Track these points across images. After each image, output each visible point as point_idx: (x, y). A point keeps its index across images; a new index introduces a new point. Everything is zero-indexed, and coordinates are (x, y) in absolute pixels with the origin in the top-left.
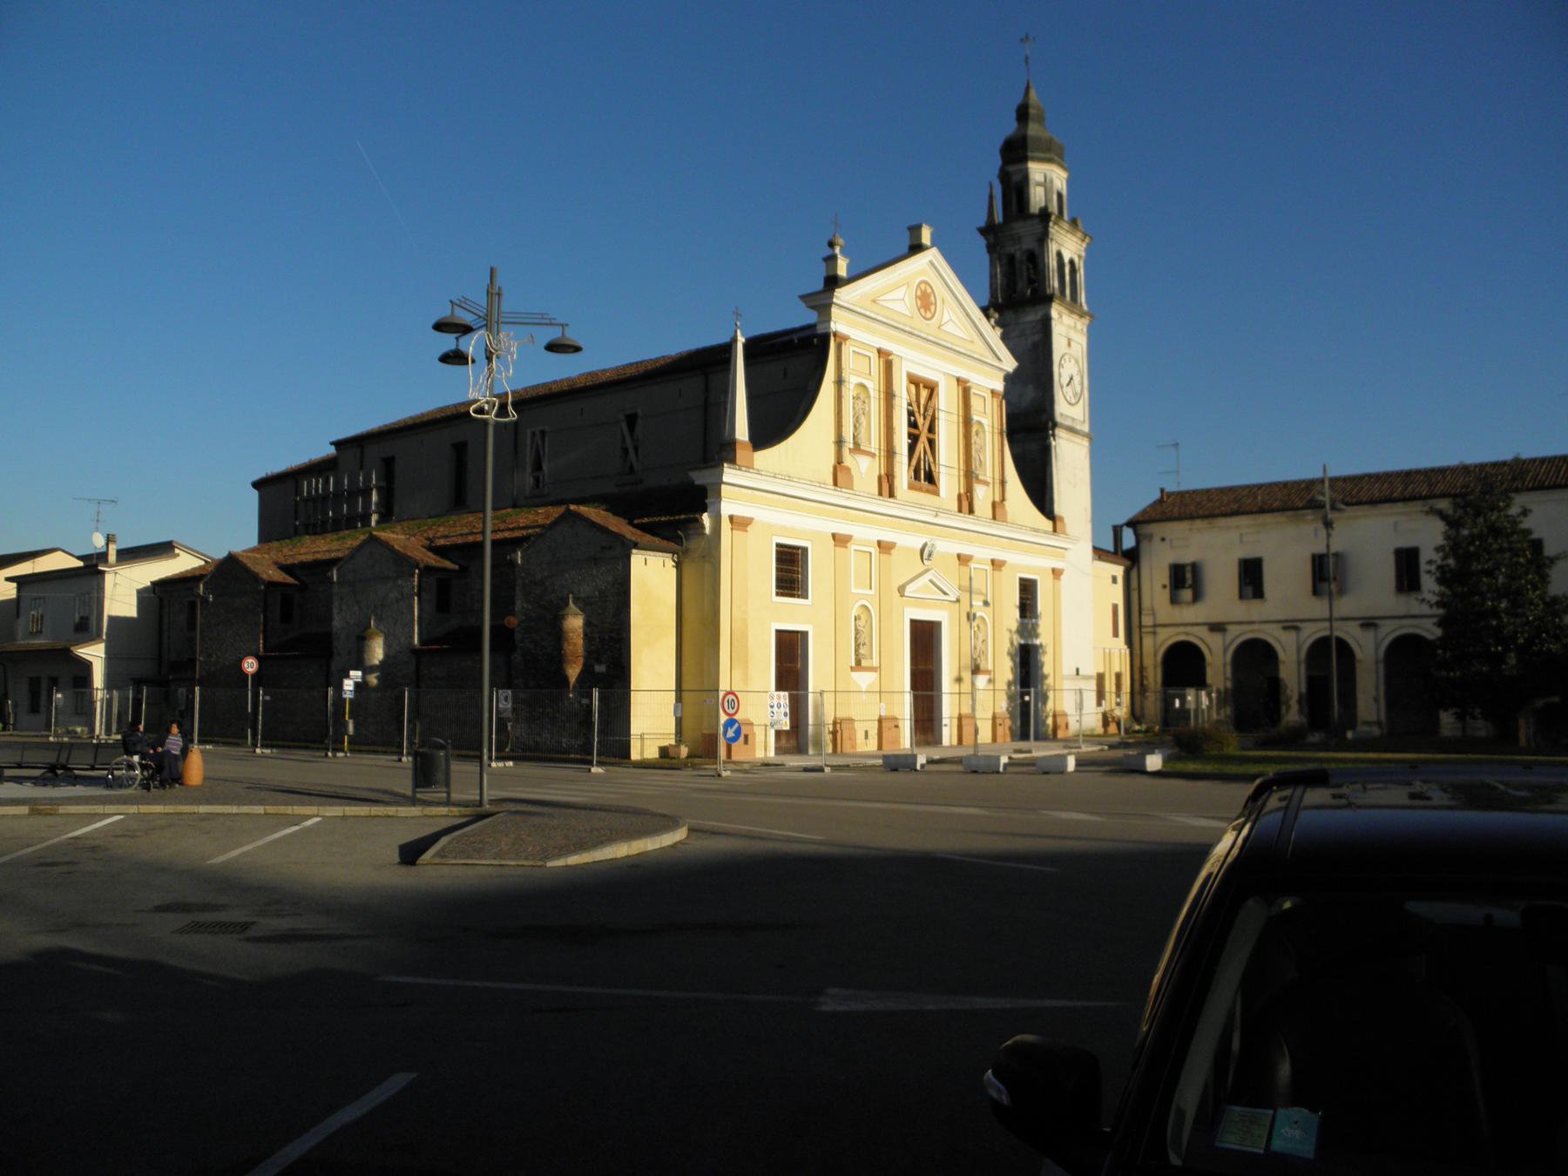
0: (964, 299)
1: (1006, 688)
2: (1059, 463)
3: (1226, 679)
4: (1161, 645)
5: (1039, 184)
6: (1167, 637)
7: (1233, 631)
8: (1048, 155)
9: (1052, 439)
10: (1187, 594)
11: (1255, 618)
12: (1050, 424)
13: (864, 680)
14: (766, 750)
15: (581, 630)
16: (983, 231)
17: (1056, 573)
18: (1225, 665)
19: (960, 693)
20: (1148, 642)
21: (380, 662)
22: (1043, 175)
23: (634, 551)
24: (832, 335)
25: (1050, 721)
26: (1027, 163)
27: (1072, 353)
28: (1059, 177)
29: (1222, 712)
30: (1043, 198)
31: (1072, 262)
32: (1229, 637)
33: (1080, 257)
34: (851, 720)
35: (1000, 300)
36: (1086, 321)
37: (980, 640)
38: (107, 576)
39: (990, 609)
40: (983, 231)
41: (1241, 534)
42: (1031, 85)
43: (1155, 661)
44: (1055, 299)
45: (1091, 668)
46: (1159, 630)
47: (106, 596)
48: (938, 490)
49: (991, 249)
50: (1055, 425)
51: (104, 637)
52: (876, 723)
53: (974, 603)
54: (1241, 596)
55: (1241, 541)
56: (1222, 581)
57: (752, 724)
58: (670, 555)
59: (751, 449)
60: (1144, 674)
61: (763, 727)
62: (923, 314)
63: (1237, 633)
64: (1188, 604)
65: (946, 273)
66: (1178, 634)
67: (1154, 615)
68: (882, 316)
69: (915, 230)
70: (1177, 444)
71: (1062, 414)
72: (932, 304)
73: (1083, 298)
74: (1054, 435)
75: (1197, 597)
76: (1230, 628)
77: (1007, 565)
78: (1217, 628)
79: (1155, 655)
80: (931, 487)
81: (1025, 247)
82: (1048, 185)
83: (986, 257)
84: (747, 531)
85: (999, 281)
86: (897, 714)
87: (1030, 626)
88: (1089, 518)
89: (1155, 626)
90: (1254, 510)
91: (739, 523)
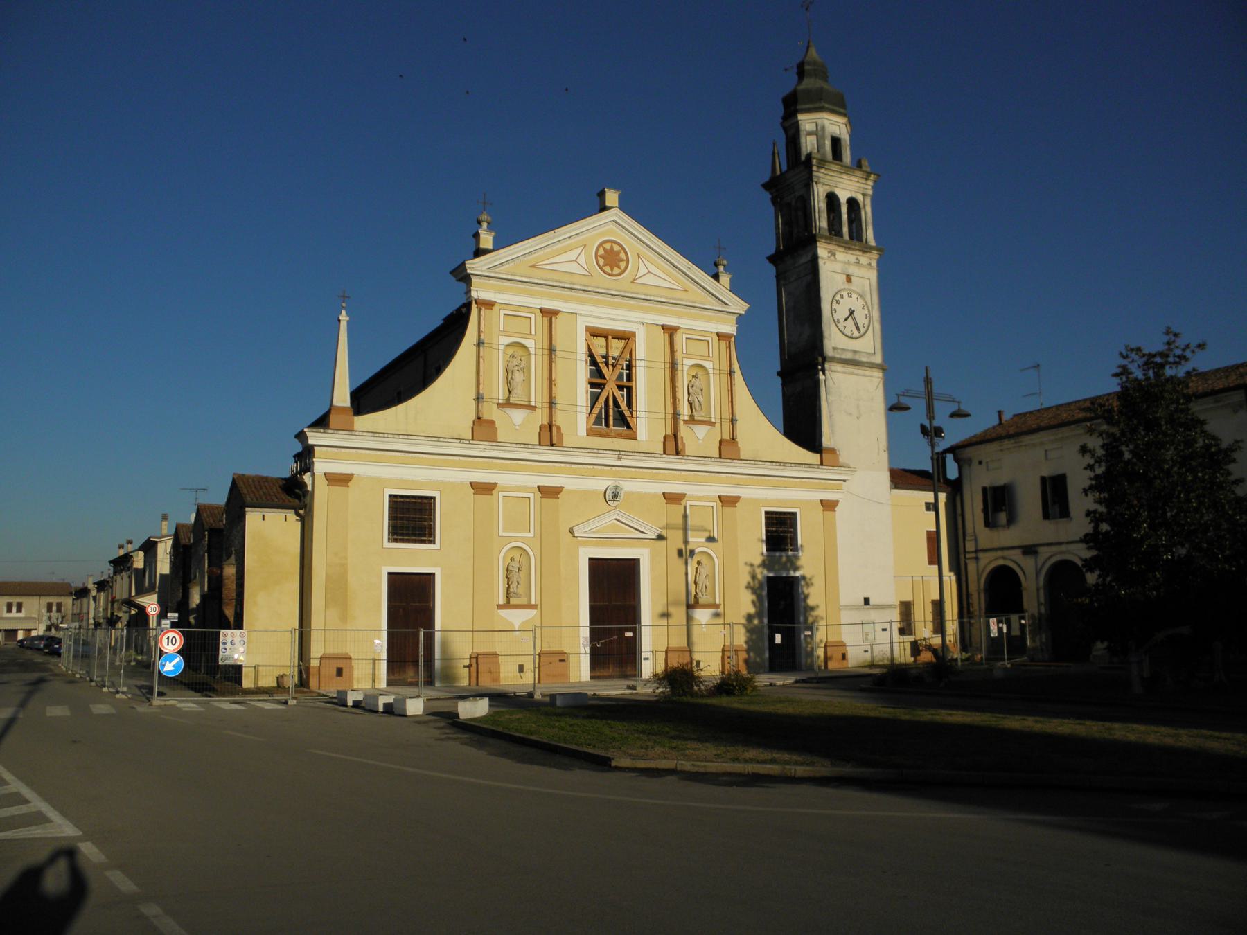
0: (667, 253)
1: (743, 621)
2: (831, 398)
3: (1040, 604)
4: (983, 571)
5: (810, 133)
6: (988, 562)
7: (1044, 552)
8: (817, 105)
9: (821, 373)
10: (1002, 517)
11: (1063, 539)
12: (820, 359)
13: (516, 618)
14: (374, 681)
15: (234, 578)
16: (766, 186)
18: (1038, 590)
19: (724, 624)
20: (972, 567)
21: (197, 605)
22: (815, 124)
23: (247, 509)
24: (474, 302)
25: (820, 652)
26: (797, 117)
27: (854, 288)
28: (835, 125)
29: (1037, 639)
30: (816, 146)
31: (852, 202)
32: (1041, 559)
33: (864, 195)
34: (495, 655)
35: (781, 248)
36: (874, 255)
37: (703, 575)
38: (159, 545)
39: (718, 546)
40: (766, 186)
41: (1046, 451)
42: (811, 44)
43: (979, 586)
44: (818, 239)
45: (889, 594)
46: (981, 555)
47: (158, 559)
48: (635, 433)
49: (774, 201)
50: (824, 359)
51: (157, 590)
52: (664, 653)
53: (690, 539)
54: (1046, 516)
55: (1046, 458)
56: (1029, 500)
57: (350, 658)
58: (293, 511)
59: (352, 413)
60: (970, 601)
63: (1049, 554)
64: (1004, 527)
65: (636, 230)
66: (996, 559)
67: (976, 540)
69: (602, 194)
70: (1038, 365)
71: (834, 349)
72: (605, 265)
73: (869, 234)
74: (823, 371)
75: (1011, 520)
76: (1041, 549)
78: (1029, 550)
79: (979, 580)
80: (629, 432)
81: (797, 194)
82: (820, 133)
83: (771, 209)
84: (348, 486)
85: (781, 231)
87: (784, 559)
88: (884, 443)
89: (977, 551)
91: (338, 480)
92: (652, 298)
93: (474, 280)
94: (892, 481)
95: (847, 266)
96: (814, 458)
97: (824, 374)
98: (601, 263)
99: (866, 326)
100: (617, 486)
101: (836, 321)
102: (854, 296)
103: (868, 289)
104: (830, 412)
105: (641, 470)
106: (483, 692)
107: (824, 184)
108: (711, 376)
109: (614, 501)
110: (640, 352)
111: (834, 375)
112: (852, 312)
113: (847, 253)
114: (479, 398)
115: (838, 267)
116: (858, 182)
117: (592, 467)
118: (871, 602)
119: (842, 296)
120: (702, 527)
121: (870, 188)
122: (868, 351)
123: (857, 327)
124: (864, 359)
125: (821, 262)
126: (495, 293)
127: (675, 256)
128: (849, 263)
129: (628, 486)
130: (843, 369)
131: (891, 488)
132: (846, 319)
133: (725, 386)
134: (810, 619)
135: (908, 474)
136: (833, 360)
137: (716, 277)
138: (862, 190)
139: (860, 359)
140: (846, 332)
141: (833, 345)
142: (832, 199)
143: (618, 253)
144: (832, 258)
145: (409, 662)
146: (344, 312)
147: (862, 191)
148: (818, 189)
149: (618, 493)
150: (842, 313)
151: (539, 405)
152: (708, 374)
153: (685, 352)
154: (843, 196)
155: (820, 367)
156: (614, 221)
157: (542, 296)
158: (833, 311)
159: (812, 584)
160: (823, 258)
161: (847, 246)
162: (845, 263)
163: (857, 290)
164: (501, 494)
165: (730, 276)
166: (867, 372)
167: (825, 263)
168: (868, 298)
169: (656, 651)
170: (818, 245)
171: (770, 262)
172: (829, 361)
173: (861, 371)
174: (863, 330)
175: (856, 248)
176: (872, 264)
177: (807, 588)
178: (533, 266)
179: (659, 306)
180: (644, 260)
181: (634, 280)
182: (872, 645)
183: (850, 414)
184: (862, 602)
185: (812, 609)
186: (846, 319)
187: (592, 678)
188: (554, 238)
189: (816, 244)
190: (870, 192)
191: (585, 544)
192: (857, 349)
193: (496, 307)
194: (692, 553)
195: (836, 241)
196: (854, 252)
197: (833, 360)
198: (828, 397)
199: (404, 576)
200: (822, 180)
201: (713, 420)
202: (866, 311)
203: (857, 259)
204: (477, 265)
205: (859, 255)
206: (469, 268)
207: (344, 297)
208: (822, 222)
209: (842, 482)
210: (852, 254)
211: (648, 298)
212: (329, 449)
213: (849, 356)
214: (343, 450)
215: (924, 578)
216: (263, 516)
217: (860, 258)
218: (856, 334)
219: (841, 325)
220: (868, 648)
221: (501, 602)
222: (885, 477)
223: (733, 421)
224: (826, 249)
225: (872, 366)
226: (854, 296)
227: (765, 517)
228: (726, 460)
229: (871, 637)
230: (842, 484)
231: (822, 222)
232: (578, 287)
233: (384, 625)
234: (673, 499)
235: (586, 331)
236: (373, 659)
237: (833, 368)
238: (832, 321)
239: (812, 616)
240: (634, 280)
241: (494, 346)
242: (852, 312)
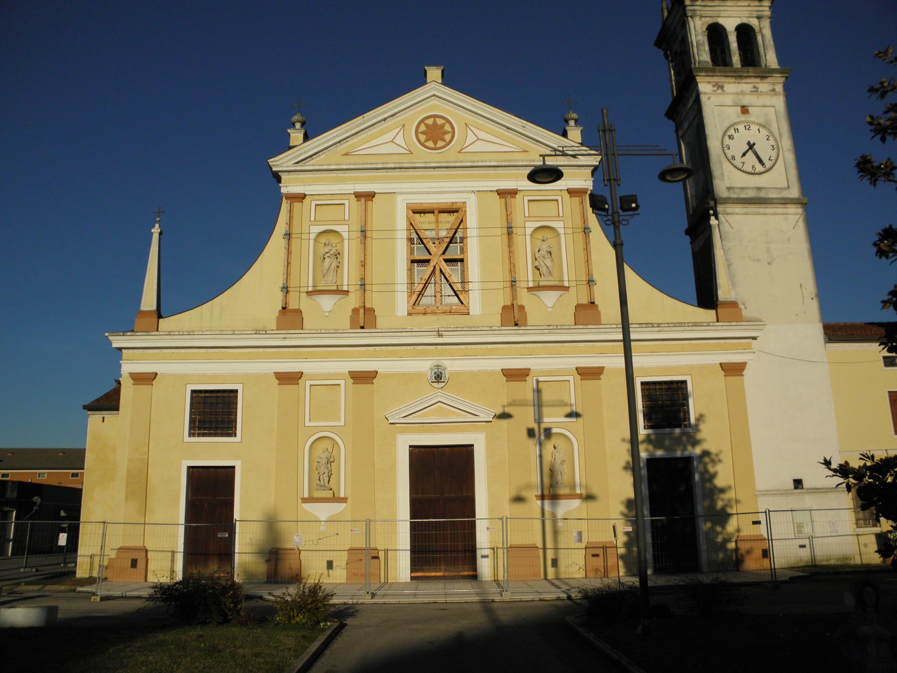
9: (713, 218)
12: (712, 203)
13: (323, 511)
17: (734, 370)
21: (852, 467)
33: (759, 18)
61: (170, 554)
62: (444, 143)
68: (436, 162)
71: (729, 189)
72: (435, 143)
73: (770, 58)
74: (716, 216)
77: (605, 371)
86: (379, 543)
90: (363, 270)
91: (145, 379)
92: (480, 164)
93: (284, 177)
94: (826, 334)
95: (740, 97)
96: (708, 315)
97: (717, 218)
98: (444, 143)
99: (773, 158)
100: (438, 366)
101: (730, 158)
102: (754, 128)
103: (772, 116)
104: (727, 260)
105: (473, 346)
106: (25, 601)
107: (701, 17)
108: (562, 237)
109: (438, 382)
110: (472, 220)
111: (731, 218)
112: (751, 146)
113: (738, 83)
114: (286, 289)
115: (728, 100)
116: (749, 6)
117: (412, 347)
118: (806, 484)
119: (736, 130)
120: (562, 401)
121: (768, 8)
122: (779, 186)
123: (760, 161)
124: (773, 195)
125: (703, 98)
126: (305, 185)
127: (505, 117)
128: (743, 93)
129: (451, 365)
130: (745, 210)
131: (826, 342)
132: (744, 154)
133: (581, 245)
134: (720, 504)
135: (871, 327)
136: (727, 201)
137: (564, 134)
138: (755, 13)
139: (766, 196)
140: (744, 168)
141: (728, 185)
142: (716, 33)
143: (435, 123)
144: (720, 91)
145: (213, 554)
146: (157, 226)
147: (755, 14)
148: (694, 23)
149: (441, 373)
150: (738, 146)
151: (351, 289)
152: (559, 235)
153: (527, 215)
154: (730, 24)
155: (711, 212)
156: (434, 95)
157: (355, 180)
158: (724, 148)
159: (720, 461)
160: (705, 93)
161: (737, 74)
162: (737, 94)
163: (758, 121)
164: (308, 383)
165: (581, 128)
166: (780, 210)
167: (709, 98)
168: (775, 128)
169: (388, 550)
170: (698, 81)
171: (669, 118)
172: (721, 203)
173: (769, 210)
174: (768, 164)
175: (751, 74)
176: (777, 90)
177: (713, 466)
178: (346, 154)
179: (492, 171)
180: (471, 127)
181: (461, 150)
182: (811, 538)
183: (758, 260)
184: (792, 485)
185: (722, 491)
186: (744, 154)
187: (412, 578)
188: (364, 123)
189: (696, 80)
190: (768, 13)
191: (403, 431)
192: (762, 186)
193: (308, 199)
194: (548, 433)
195: (720, 71)
196: (749, 80)
197: (727, 201)
198: (724, 243)
199: (211, 470)
200: (698, 13)
201: (566, 284)
202: (772, 142)
203: (755, 87)
204: (281, 162)
205: (757, 83)
206: (274, 165)
207: (159, 212)
208: (702, 53)
209: (750, 340)
210: (745, 83)
211: (476, 164)
212: (136, 351)
213: (751, 194)
214: (148, 351)
215: (888, 451)
216: (103, 418)
217: (757, 85)
218: (759, 168)
219: (738, 162)
220: (806, 542)
221: (306, 495)
222: (817, 331)
223: (590, 282)
224: (709, 83)
225: (785, 202)
226: (754, 128)
227: (642, 390)
228: (606, 326)
229: (807, 530)
230: (750, 343)
231: (702, 53)
232: (392, 166)
233: (182, 519)
234: (515, 375)
235: (408, 208)
236: (603, 547)
237: (729, 210)
238: (723, 159)
239: (723, 500)
240: (461, 150)
241: (304, 236)
242: (751, 146)
